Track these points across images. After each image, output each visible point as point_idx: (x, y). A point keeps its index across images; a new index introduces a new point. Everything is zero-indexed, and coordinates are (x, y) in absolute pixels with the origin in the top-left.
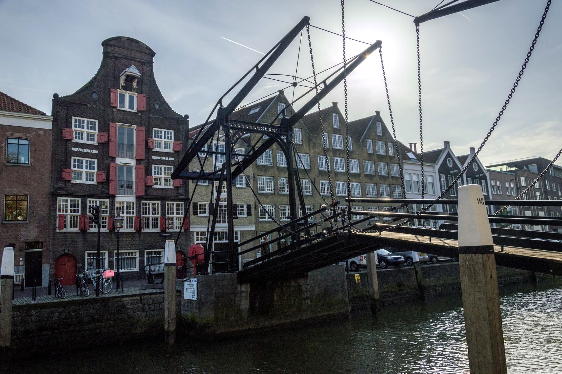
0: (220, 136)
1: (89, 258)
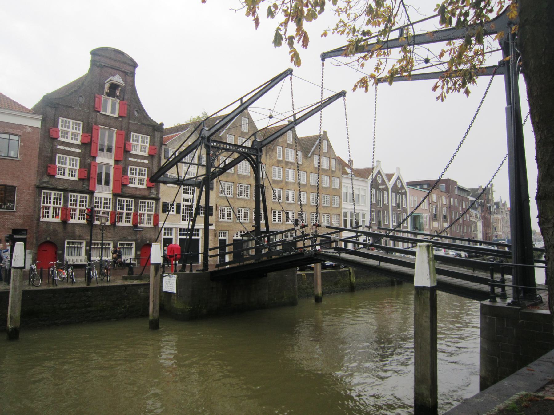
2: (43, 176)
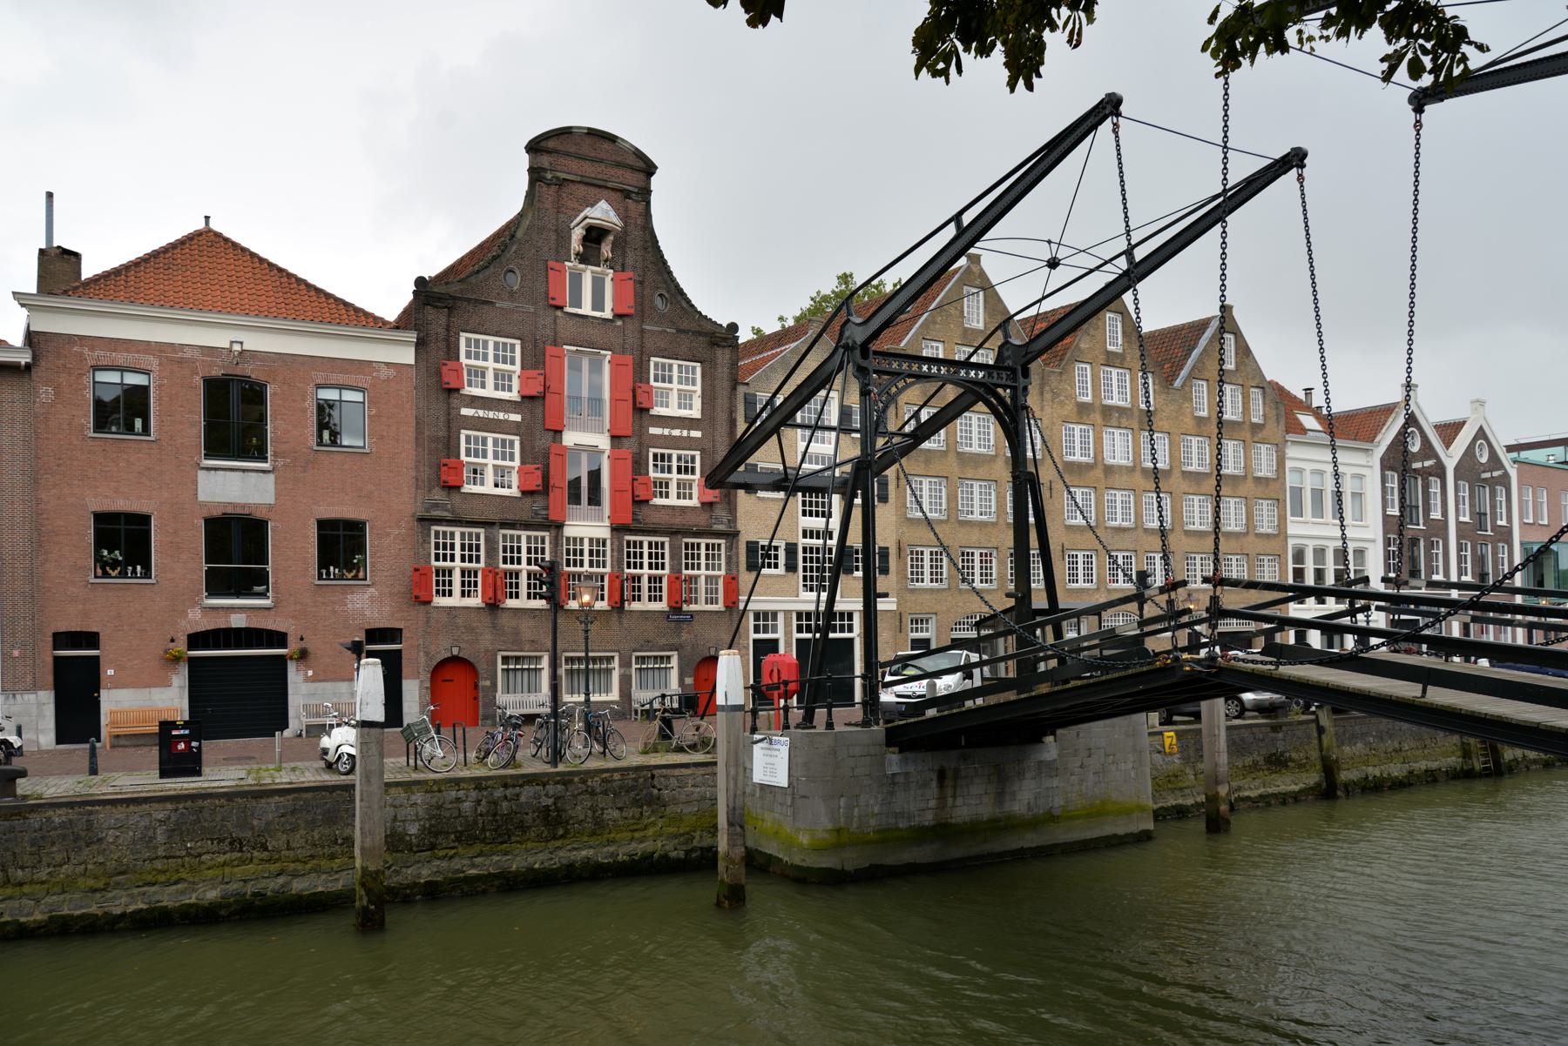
1: (505, 667)
2: (430, 491)
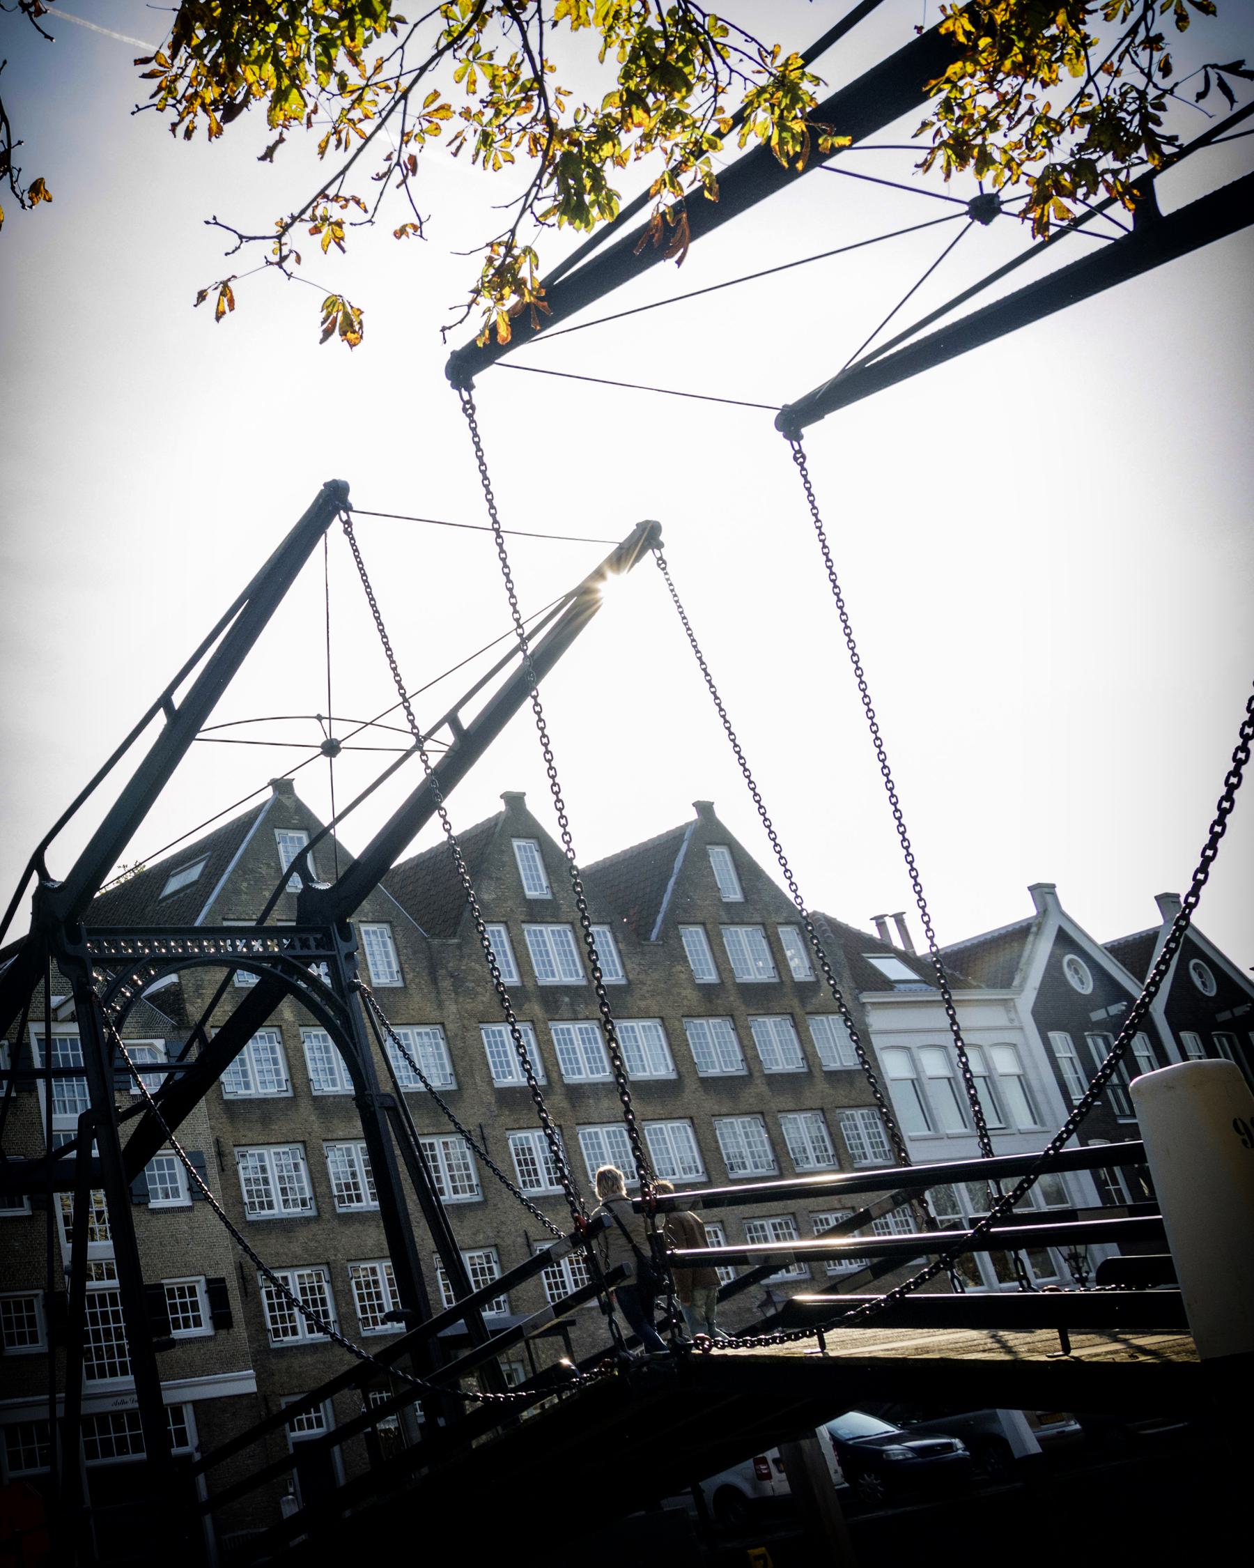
0: (55, 1000)
